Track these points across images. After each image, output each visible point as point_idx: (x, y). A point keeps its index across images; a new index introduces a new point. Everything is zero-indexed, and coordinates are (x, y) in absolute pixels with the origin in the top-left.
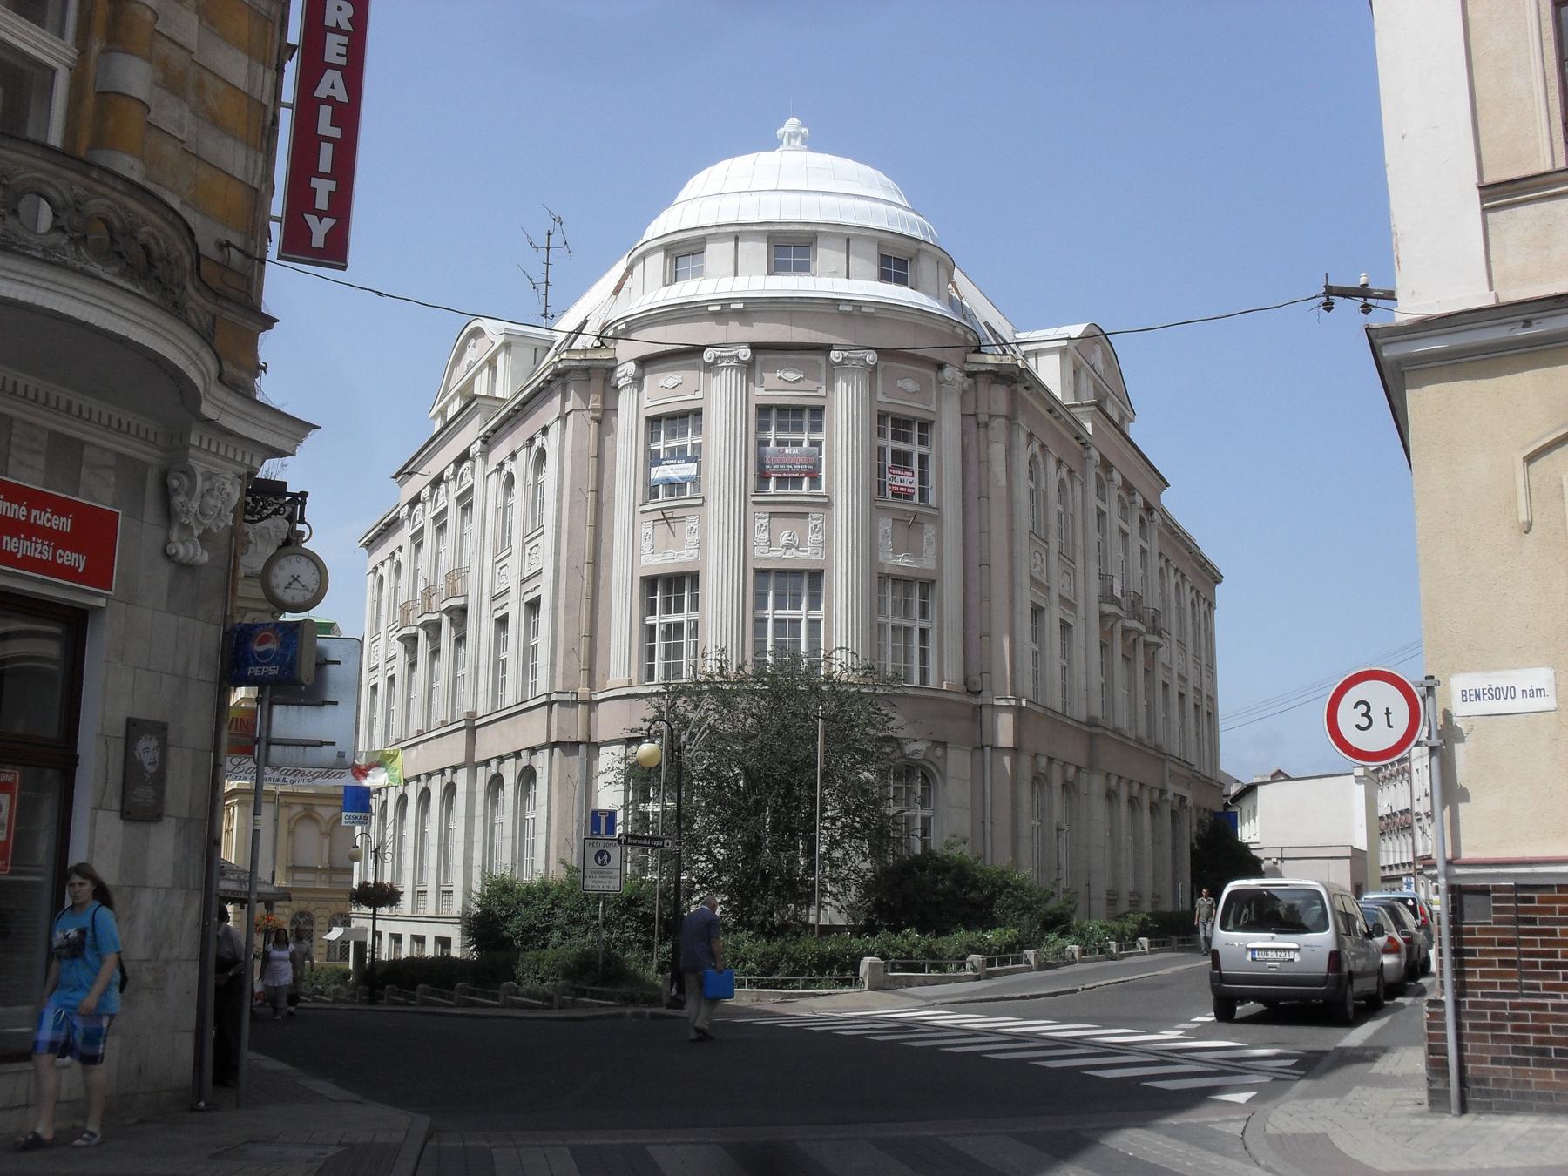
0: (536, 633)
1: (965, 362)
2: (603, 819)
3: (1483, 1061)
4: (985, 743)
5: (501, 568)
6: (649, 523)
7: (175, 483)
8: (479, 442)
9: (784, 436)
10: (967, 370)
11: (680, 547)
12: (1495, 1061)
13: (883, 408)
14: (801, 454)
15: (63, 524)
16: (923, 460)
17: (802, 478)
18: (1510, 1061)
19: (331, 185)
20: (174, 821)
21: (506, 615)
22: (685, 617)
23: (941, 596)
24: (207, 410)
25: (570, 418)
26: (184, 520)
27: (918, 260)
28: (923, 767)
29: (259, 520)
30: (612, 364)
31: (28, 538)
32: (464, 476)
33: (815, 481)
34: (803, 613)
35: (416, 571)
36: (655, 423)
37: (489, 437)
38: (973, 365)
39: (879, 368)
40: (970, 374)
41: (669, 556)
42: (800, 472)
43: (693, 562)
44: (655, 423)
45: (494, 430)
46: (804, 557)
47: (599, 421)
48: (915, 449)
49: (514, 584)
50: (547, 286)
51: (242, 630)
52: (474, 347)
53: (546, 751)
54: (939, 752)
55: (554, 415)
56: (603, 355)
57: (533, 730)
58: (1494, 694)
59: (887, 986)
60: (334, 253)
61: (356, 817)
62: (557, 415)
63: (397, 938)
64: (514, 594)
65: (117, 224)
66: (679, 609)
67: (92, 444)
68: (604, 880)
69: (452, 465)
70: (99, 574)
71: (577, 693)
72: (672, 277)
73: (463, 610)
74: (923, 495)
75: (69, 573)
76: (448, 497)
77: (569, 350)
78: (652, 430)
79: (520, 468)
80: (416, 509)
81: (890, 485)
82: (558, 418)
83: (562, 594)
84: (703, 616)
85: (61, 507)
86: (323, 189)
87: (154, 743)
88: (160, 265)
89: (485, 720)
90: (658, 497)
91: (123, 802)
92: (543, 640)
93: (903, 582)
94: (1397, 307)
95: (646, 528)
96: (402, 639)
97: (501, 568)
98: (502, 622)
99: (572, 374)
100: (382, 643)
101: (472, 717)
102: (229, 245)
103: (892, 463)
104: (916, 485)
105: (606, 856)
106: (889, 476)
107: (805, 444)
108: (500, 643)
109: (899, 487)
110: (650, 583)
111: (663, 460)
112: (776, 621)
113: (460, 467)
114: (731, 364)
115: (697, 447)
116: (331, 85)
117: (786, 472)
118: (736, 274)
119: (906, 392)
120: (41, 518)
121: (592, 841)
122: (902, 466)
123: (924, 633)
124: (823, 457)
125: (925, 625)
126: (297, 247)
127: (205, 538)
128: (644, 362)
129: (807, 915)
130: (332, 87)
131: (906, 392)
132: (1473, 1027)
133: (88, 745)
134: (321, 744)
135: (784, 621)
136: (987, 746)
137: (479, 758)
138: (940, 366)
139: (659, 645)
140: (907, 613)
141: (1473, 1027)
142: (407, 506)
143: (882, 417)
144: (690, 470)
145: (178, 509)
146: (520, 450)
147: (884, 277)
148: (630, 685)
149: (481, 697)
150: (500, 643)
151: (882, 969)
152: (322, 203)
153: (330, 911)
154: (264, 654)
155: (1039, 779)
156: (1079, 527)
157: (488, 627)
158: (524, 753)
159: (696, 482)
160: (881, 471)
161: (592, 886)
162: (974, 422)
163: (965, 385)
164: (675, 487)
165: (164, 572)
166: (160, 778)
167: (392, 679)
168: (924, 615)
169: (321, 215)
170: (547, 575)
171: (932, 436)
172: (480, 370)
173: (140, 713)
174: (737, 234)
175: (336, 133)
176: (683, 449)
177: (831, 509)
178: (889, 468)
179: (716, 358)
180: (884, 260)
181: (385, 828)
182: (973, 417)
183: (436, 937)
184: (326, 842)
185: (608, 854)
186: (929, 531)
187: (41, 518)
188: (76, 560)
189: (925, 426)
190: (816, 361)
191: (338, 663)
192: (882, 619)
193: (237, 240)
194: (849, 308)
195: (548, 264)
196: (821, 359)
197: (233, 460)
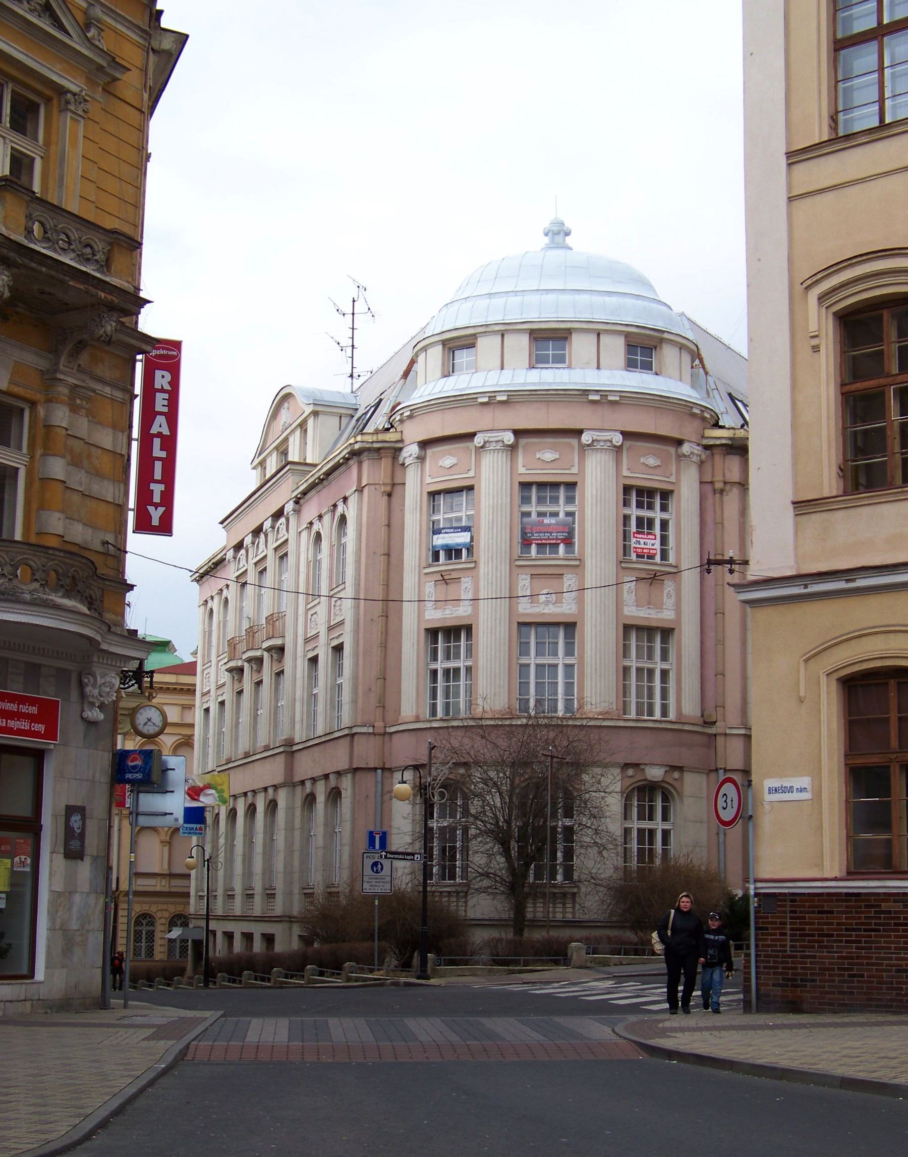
0: (340, 674)
1: (703, 437)
2: (377, 837)
3: (768, 985)
4: (719, 766)
5: (312, 615)
6: (431, 583)
7: (86, 680)
8: (291, 502)
9: (542, 509)
10: (704, 443)
12: (774, 985)
13: (629, 482)
14: (557, 524)
15: (34, 710)
16: (664, 524)
17: (559, 544)
18: (780, 985)
19: (162, 487)
20: (89, 858)
21: (317, 656)
22: (461, 664)
24: (104, 646)
25: (366, 490)
26: (91, 699)
27: (661, 348)
28: (663, 788)
29: (128, 688)
30: (400, 445)
31: (18, 720)
32: (280, 529)
33: (568, 542)
35: (242, 608)
36: (436, 496)
37: (300, 498)
38: (710, 440)
39: (625, 448)
40: (707, 447)
41: (447, 612)
42: (557, 539)
43: (469, 616)
44: (436, 496)
45: (304, 493)
46: (565, 609)
47: (390, 495)
48: (657, 515)
49: (323, 630)
50: (353, 348)
51: (121, 753)
52: (288, 409)
53: (349, 776)
54: (676, 775)
55: (352, 488)
56: (391, 436)
57: (338, 758)
59: (588, 965)
60: (165, 527)
61: (192, 829)
62: (355, 489)
63: (229, 936)
64: (323, 638)
65: (60, 571)
66: (457, 656)
67: (45, 665)
68: (378, 884)
69: (270, 519)
70: (51, 734)
71: (374, 727)
72: (449, 371)
73: (281, 649)
74: (664, 555)
75: (37, 734)
76: (266, 548)
77: (361, 432)
78: (434, 502)
79: (326, 527)
80: (240, 554)
81: (634, 548)
82: (355, 491)
84: (476, 662)
85: (32, 701)
86: (157, 489)
87: (79, 817)
88: (79, 584)
89: (300, 747)
90: (439, 561)
91: (65, 849)
92: (345, 680)
93: (647, 631)
96: (230, 670)
97: (312, 615)
98: (314, 660)
99: (366, 454)
100: (213, 670)
101: (289, 743)
102: (108, 543)
103: (637, 528)
104: (658, 546)
105: (379, 866)
106: (633, 540)
107: (562, 515)
108: (312, 678)
109: (643, 549)
110: (433, 633)
111: (443, 529)
112: (537, 665)
113: (277, 521)
114: (498, 447)
116: (160, 425)
117: (545, 539)
118: (502, 368)
120: (24, 709)
121: (369, 855)
122: (646, 531)
123: (665, 674)
124: (576, 526)
125: (665, 666)
126: (144, 526)
127: (102, 707)
128: (425, 444)
129: (554, 912)
130: (160, 426)
132: (765, 967)
133: (47, 820)
134: (166, 814)
135: (543, 665)
136: (721, 769)
137: (297, 779)
138: (679, 442)
140: (650, 657)
141: (765, 967)
142: (232, 550)
143: (627, 489)
144: (463, 538)
145: (89, 693)
146: (326, 513)
147: (631, 365)
148: (417, 720)
149: (297, 726)
150: (312, 678)
151: (584, 952)
152: (157, 499)
154: (134, 767)
157: (302, 666)
158: (332, 777)
159: (470, 549)
160: (626, 536)
161: (370, 889)
163: (703, 457)
164: (453, 552)
165: (81, 727)
166: (82, 836)
167: (222, 703)
168: (665, 657)
169: (156, 506)
170: (348, 626)
171: (672, 504)
172: (293, 431)
173: (72, 803)
174: (504, 331)
175: (163, 454)
178: (634, 533)
179: (485, 443)
181: (218, 838)
182: (710, 484)
183: (262, 934)
184: (166, 849)
185: (381, 864)
186: (669, 586)
187: (24, 709)
188: (40, 727)
189: (666, 495)
190: (570, 443)
191: (174, 769)
192: (627, 663)
193: (111, 539)
194: (597, 398)
195: (353, 329)
196: (574, 442)
197: (115, 666)
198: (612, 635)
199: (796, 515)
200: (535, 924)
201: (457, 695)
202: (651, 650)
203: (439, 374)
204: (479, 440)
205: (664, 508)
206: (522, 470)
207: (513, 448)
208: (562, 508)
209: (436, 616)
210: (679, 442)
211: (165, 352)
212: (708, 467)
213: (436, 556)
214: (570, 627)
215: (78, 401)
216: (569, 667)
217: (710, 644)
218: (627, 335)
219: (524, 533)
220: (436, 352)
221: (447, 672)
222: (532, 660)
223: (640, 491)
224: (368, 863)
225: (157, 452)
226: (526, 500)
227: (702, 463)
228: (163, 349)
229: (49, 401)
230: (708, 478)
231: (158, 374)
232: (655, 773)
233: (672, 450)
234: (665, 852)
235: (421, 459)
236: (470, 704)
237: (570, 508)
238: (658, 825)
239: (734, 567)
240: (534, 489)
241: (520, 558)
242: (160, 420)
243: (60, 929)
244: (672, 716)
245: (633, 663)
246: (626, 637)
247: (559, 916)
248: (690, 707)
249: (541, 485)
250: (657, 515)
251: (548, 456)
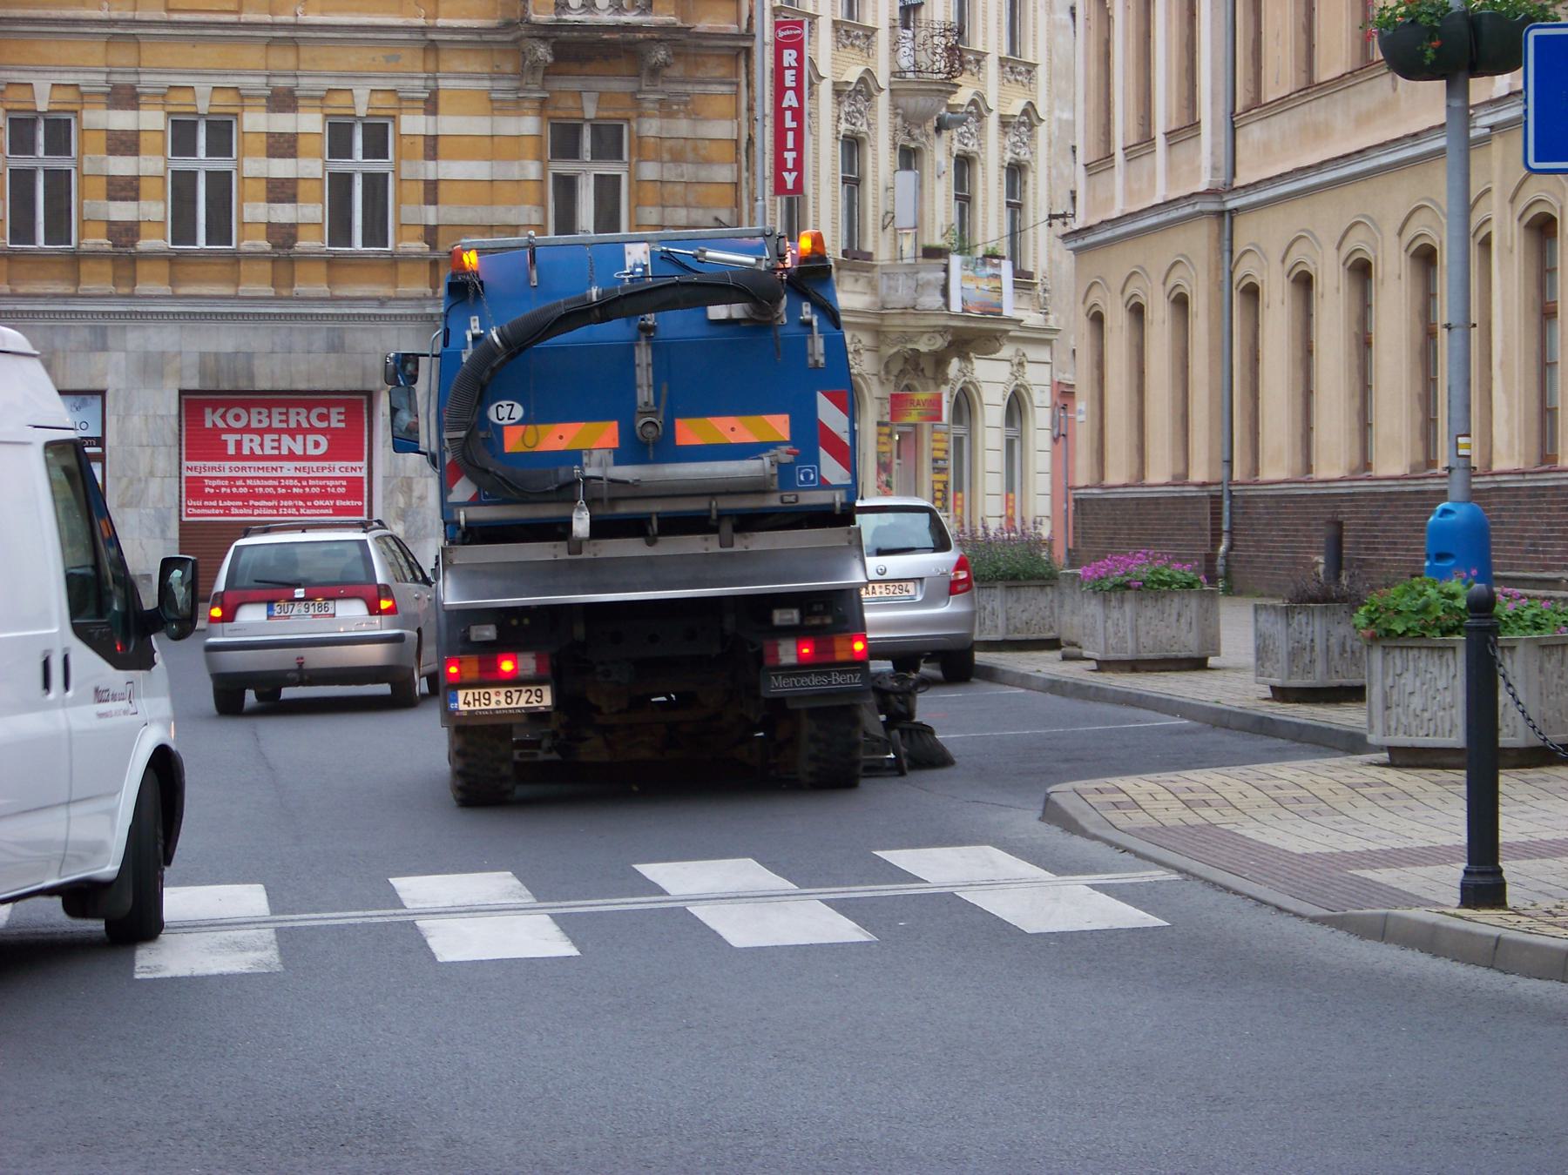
83: (366, 489)
86: (790, 156)
94: (1217, 654)
152: (790, 165)
153: (1046, 320)
169: (790, 171)
175: (794, 125)
177: (878, 495)
199: (1128, 160)
211: (791, 32)
215: (675, 107)
228: (789, 29)
229: (640, 116)
231: (786, 52)
239: (1067, 220)
242: (790, 95)
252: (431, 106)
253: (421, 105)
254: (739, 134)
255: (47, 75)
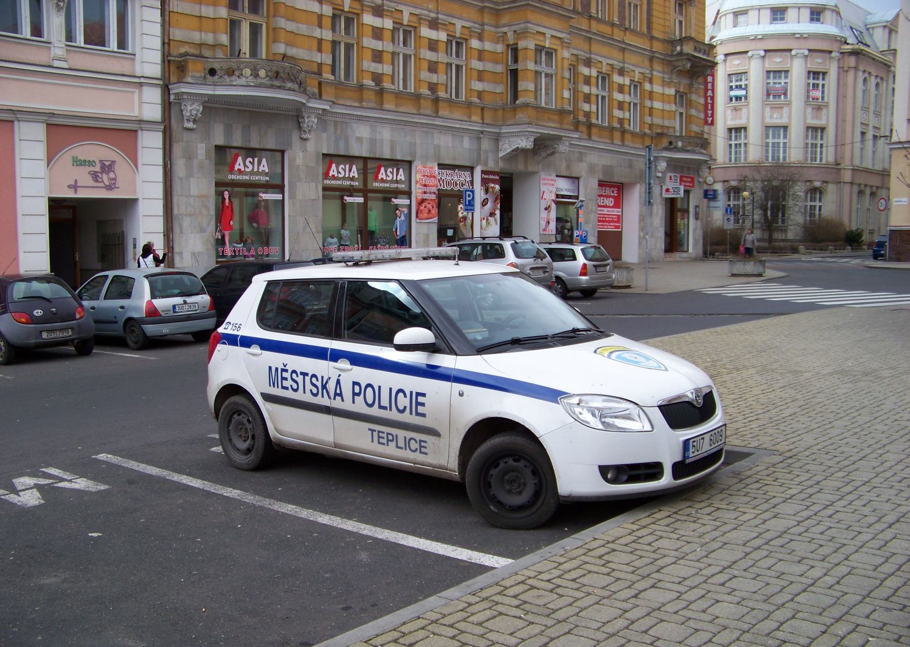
1: (841, 49)
11: (741, 118)
13: (810, 70)
16: (823, 86)
22: (742, 141)
23: (828, 134)
33: (785, 94)
34: (781, 141)
46: (784, 121)
54: (825, 184)
58: (899, 201)
70: (693, 186)
74: (823, 98)
86: (710, 112)
93: (815, 129)
95: (729, 112)
104: (820, 95)
107: (783, 84)
110: (730, 130)
115: (746, 85)
116: (710, 93)
119: (817, 63)
128: (726, 55)
131: (817, 63)
138: (831, 52)
139: (733, 149)
140: (816, 139)
143: (809, 72)
144: (743, 93)
147: (812, 20)
155: (861, 193)
156: (884, 99)
159: (746, 97)
160: (808, 91)
162: (842, 70)
164: (738, 98)
168: (822, 139)
171: (827, 77)
174: (760, 9)
176: (741, 86)
180: (812, 13)
186: (824, 111)
188: (691, 184)
189: (824, 74)
194: (798, 36)
196: (788, 54)
198: (802, 130)
200: (776, 240)
201: (740, 154)
202: (816, 136)
203: (732, 26)
204: (750, 54)
205: (823, 79)
206: (767, 66)
207: (764, 57)
208: (783, 81)
209: (732, 123)
210: (831, 52)
212: (842, 61)
213: (731, 99)
214: (785, 128)
216: (785, 144)
217: (839, 133)
218: (811, 8)
219: (767, 91)
220: (730, 17)
221: (736, 145)
222: (770, 141)
223: (814, 73)
224: (726, 218)
225: (709, 101)
226: (768, 78)
227: (839, 60)
229: (690, 93)
230: (841, 65)
232: (817, 184)
233: (827, 55)
234: (820, 214)
235: (725, 61)
236: (746, 158)
237: (786, 81)
238: (817, 204)
240: (772, 73)
241: (766, 101)
243: (694, 239)
244: (824, 162)
245: (810, 141)
246: (807, 131)
247: (780, 238)
248: (831, 159)
249: (775, 72)
250: (820, 82)
251: (778, 60)
252: (480, 38)
253: (476, 35)
254: (874, 145)
255: (409, 8)
